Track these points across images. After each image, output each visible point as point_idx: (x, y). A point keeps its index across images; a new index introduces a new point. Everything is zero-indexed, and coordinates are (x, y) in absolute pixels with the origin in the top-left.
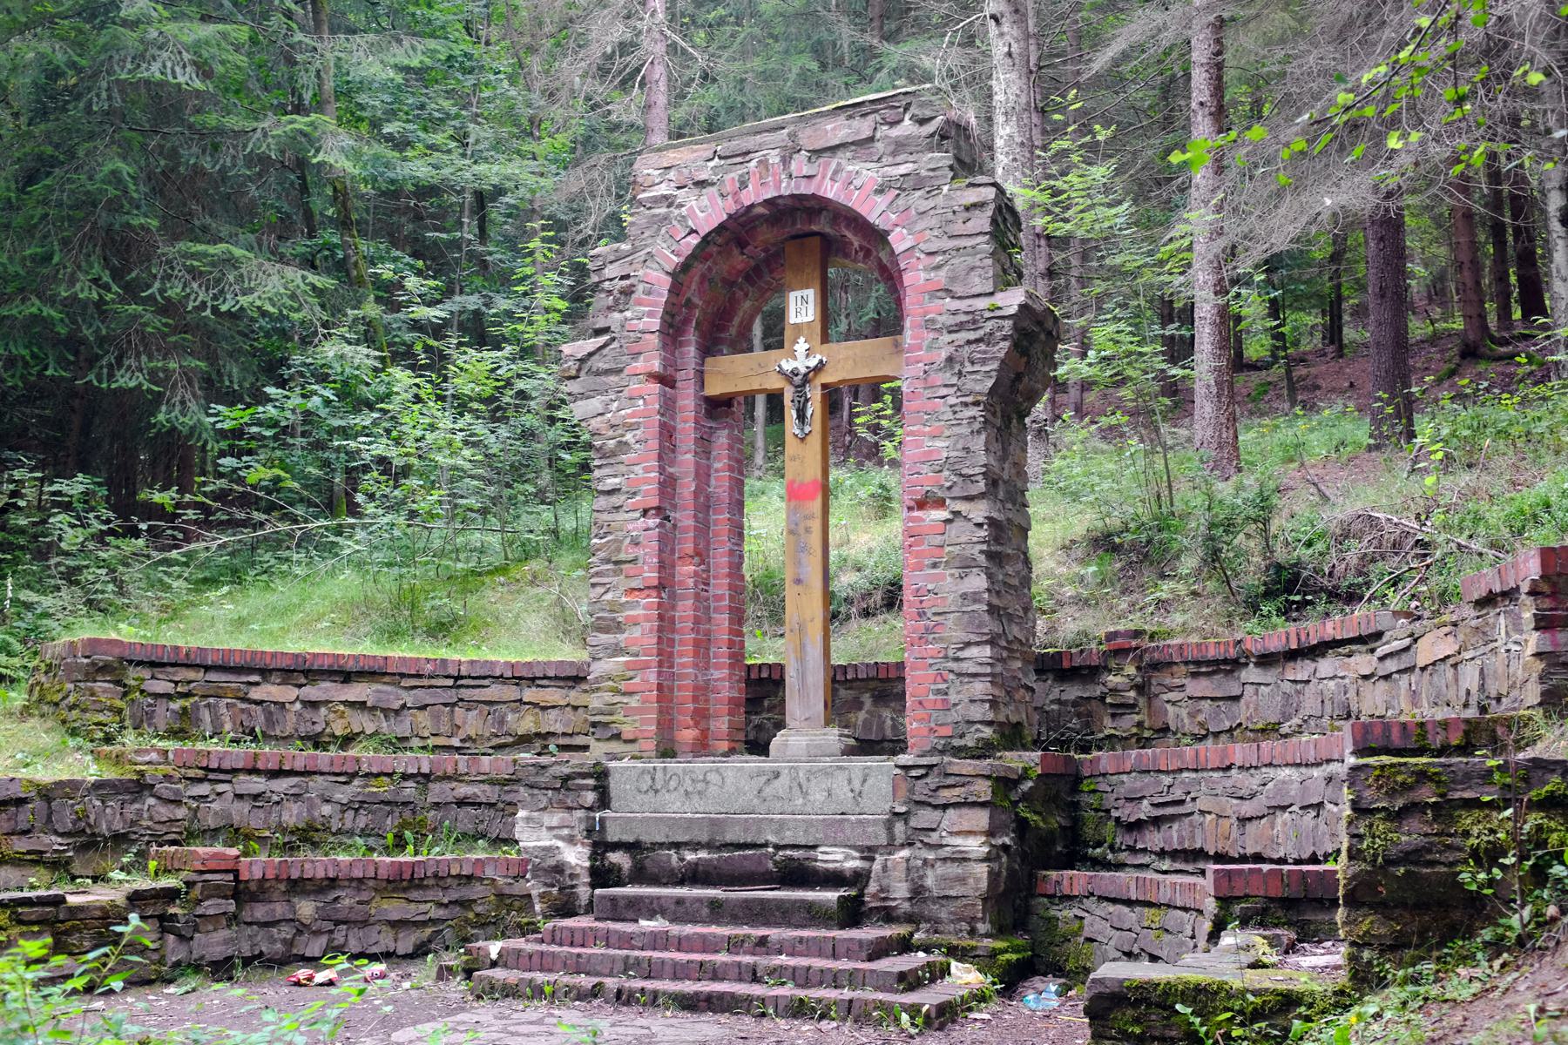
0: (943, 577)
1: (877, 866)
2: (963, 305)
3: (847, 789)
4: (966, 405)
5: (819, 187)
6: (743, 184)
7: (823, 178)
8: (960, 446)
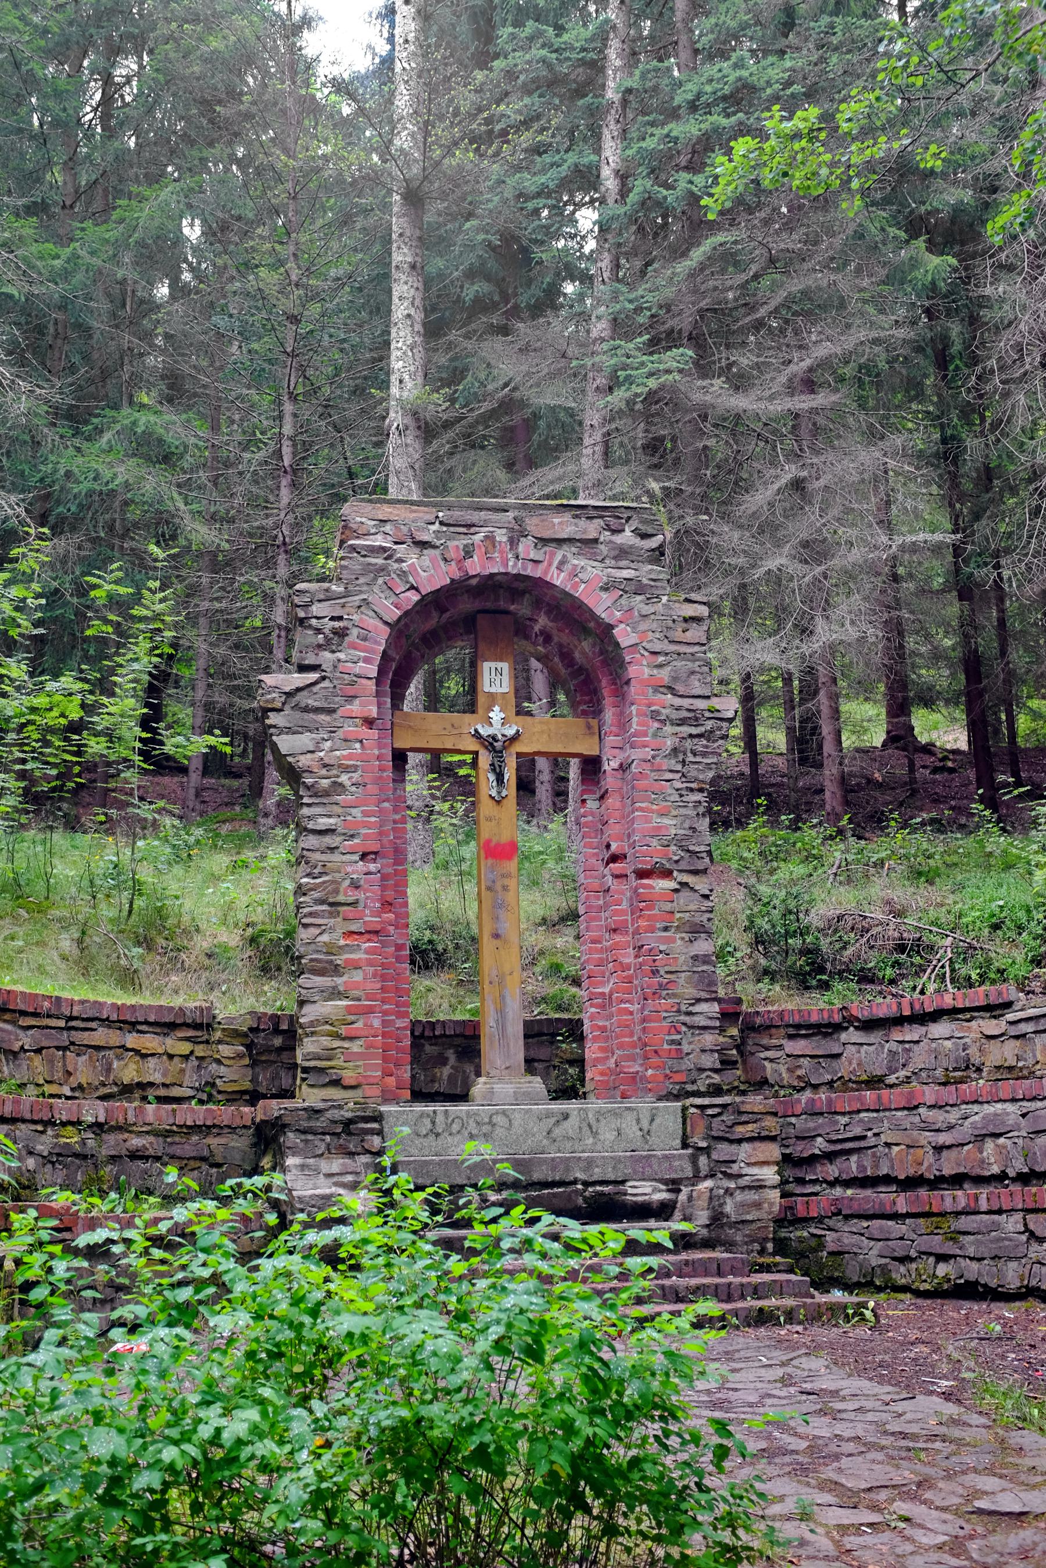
0: (674, 941)
1: (682, 1197)
2: (686, 703)
3: (635, 1128)
4: (692, 790)
5: (546, 572)
6: (468, 554)
7: (550, 565)
8: (687, 825)
